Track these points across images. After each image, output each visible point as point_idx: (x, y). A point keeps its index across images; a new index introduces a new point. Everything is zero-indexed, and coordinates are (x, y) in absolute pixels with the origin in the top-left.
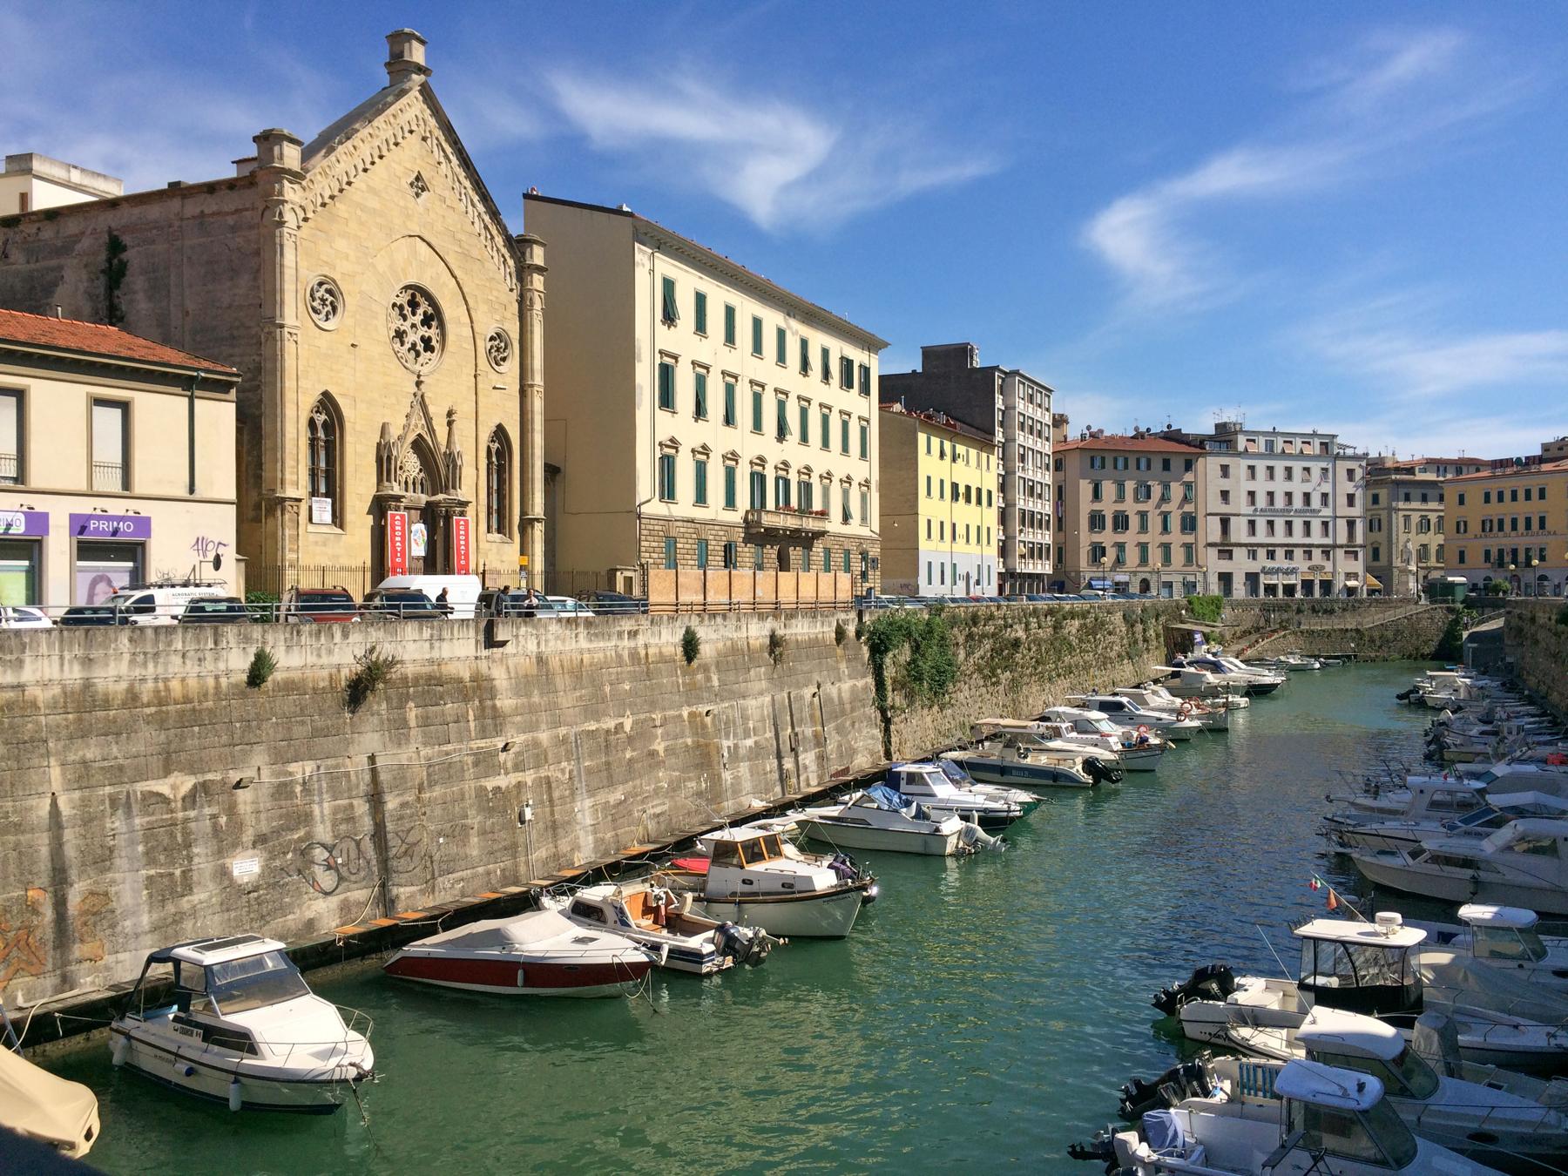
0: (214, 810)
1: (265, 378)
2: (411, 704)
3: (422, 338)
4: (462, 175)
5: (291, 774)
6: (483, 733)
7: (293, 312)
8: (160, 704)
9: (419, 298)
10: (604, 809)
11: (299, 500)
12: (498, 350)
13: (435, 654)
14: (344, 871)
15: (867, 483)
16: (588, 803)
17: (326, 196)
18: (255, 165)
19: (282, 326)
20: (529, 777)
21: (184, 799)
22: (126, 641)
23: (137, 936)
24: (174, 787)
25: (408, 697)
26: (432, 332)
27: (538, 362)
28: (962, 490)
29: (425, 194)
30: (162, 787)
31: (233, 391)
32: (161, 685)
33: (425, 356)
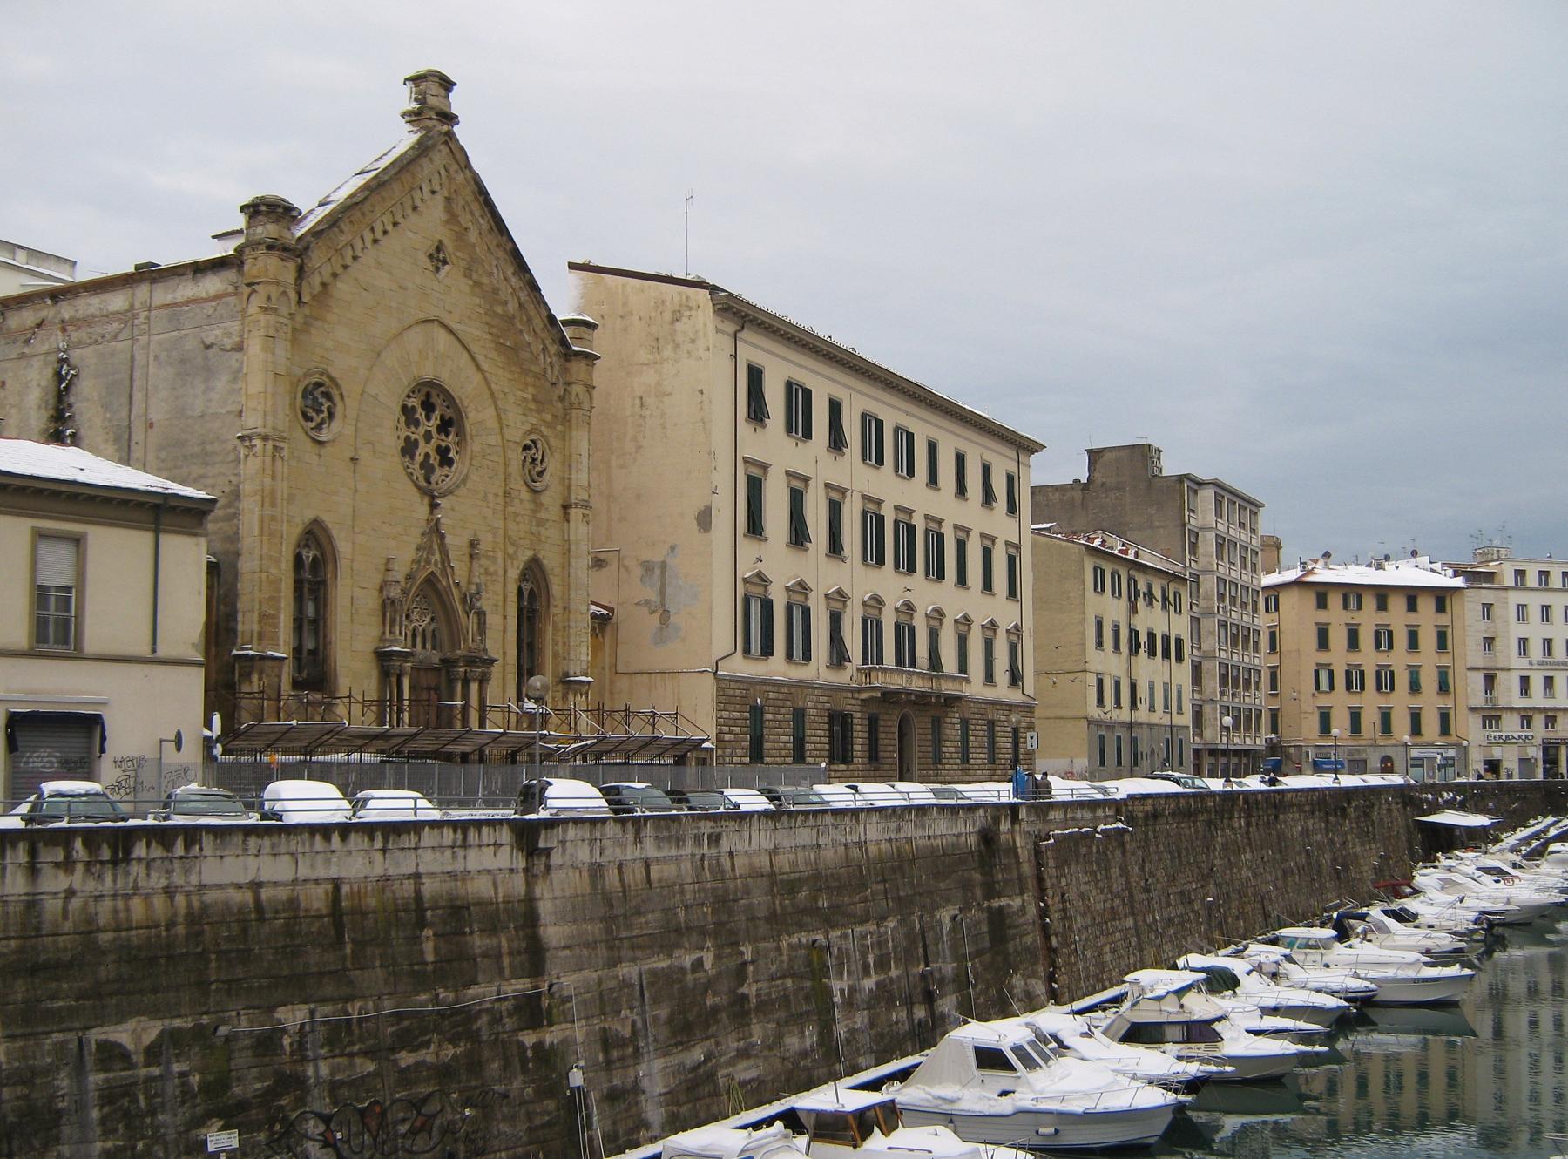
2: (428, 932)
5: (279, 1022)
8: (117, 929)
9: (436, 400)
13: (459, 866)
15: (1018, 630)
16: (658, 1064)
24: (137, 1037)
28: (1143, 639)
30: (122, 1034)
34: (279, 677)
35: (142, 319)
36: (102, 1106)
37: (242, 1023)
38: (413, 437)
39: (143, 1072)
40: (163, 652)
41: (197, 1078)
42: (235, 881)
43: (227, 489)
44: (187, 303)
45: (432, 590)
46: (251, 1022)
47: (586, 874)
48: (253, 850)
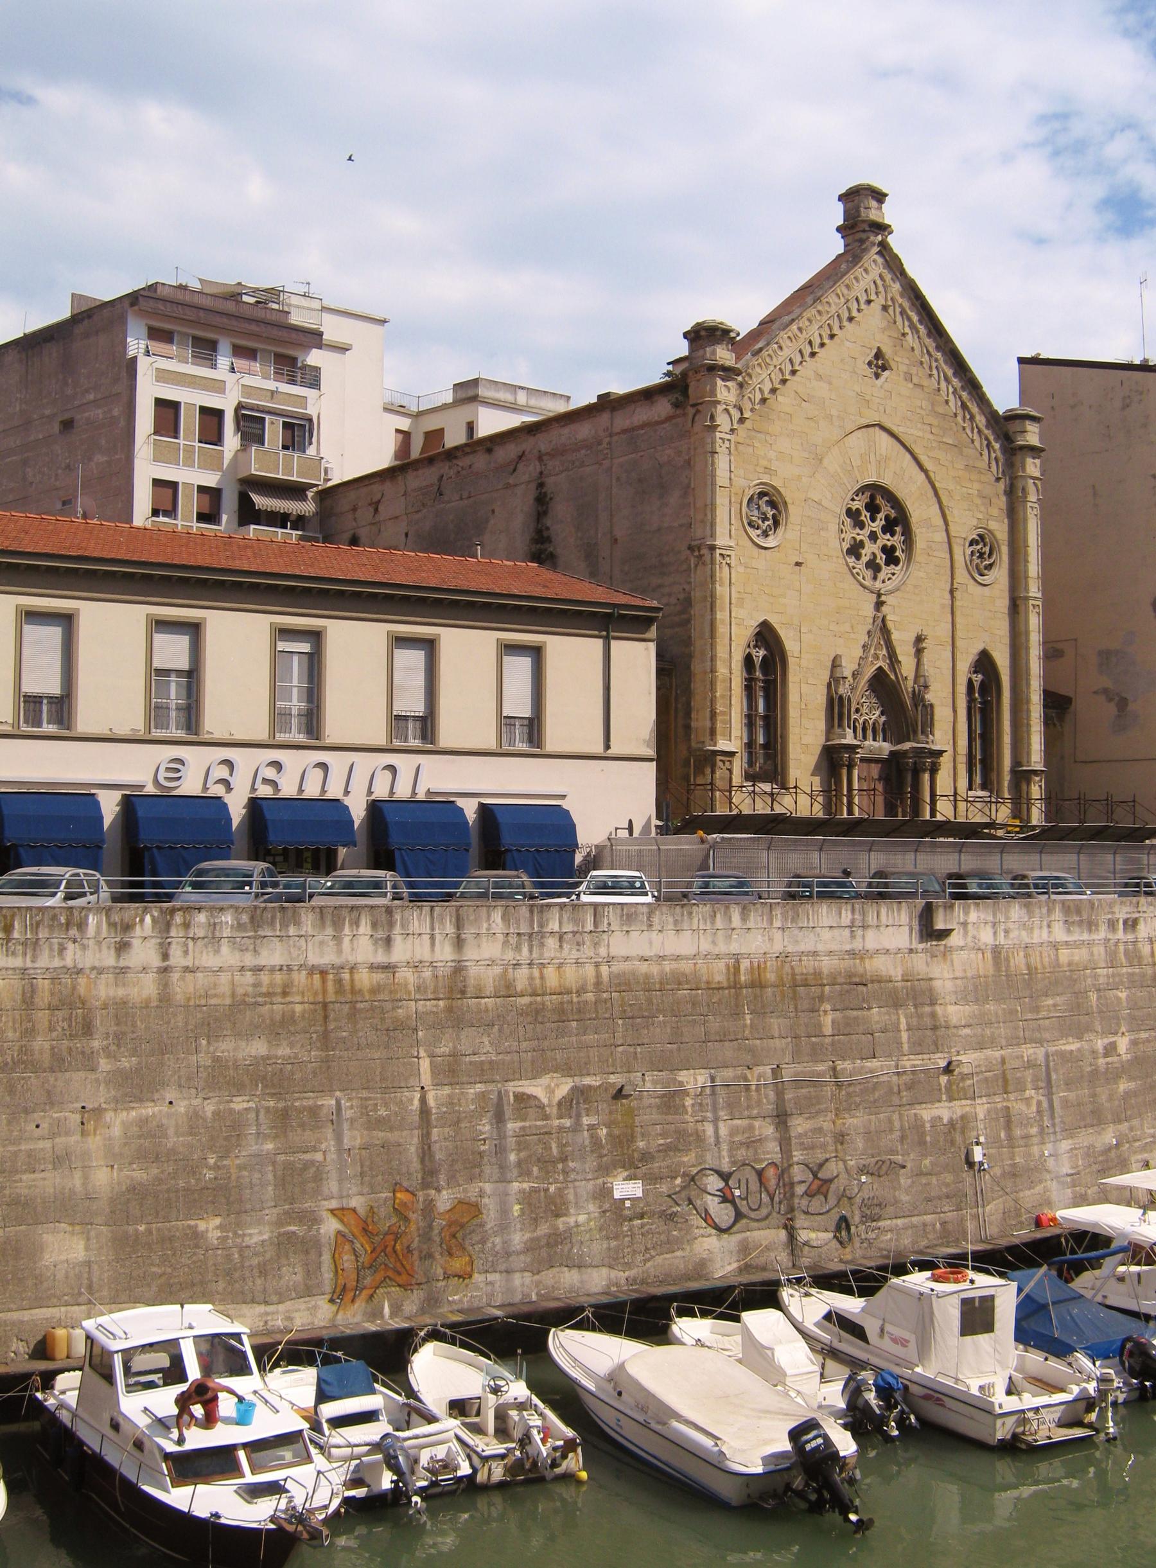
0: (593, 1120)
1: (696, 610)
3: (884, 549)
4: (930, 343)
5: (681, 1084)
6: (918, 1047)
7: (727, 531)
9: (879, 500)
10: (1088, 1155)
11: (732, 754)
12: (981, 555)
13: (857, 945)
14: (743, 1206)
17: (767, 389)
18: (685, 365)
19: (713, 548)
20: (981, 1109)
21: (560, 1104)
22: (499, 920)
23: (508, 1254)
24: (550, 1091)
25: (821, 998)
26: (897, 540)
27: (1033, 568)
29: (886, 373)
30: (536, 1088)
31: (654, 628)
32: (536, 972)
33: (885, 571)
34: (730, 771)
35: (605, 445)
36: (519, 1151)
37: (649, 1084)
38: (859, 538)
39: (556, 1122)
40: (614, 750)
41: (605, 1131)
42: (641, 953)
43: (681, 596)
44: (642, 427)
45: (883, 686)
46: (655, 1083)
47: (989, 955)
48: (657, 927)
